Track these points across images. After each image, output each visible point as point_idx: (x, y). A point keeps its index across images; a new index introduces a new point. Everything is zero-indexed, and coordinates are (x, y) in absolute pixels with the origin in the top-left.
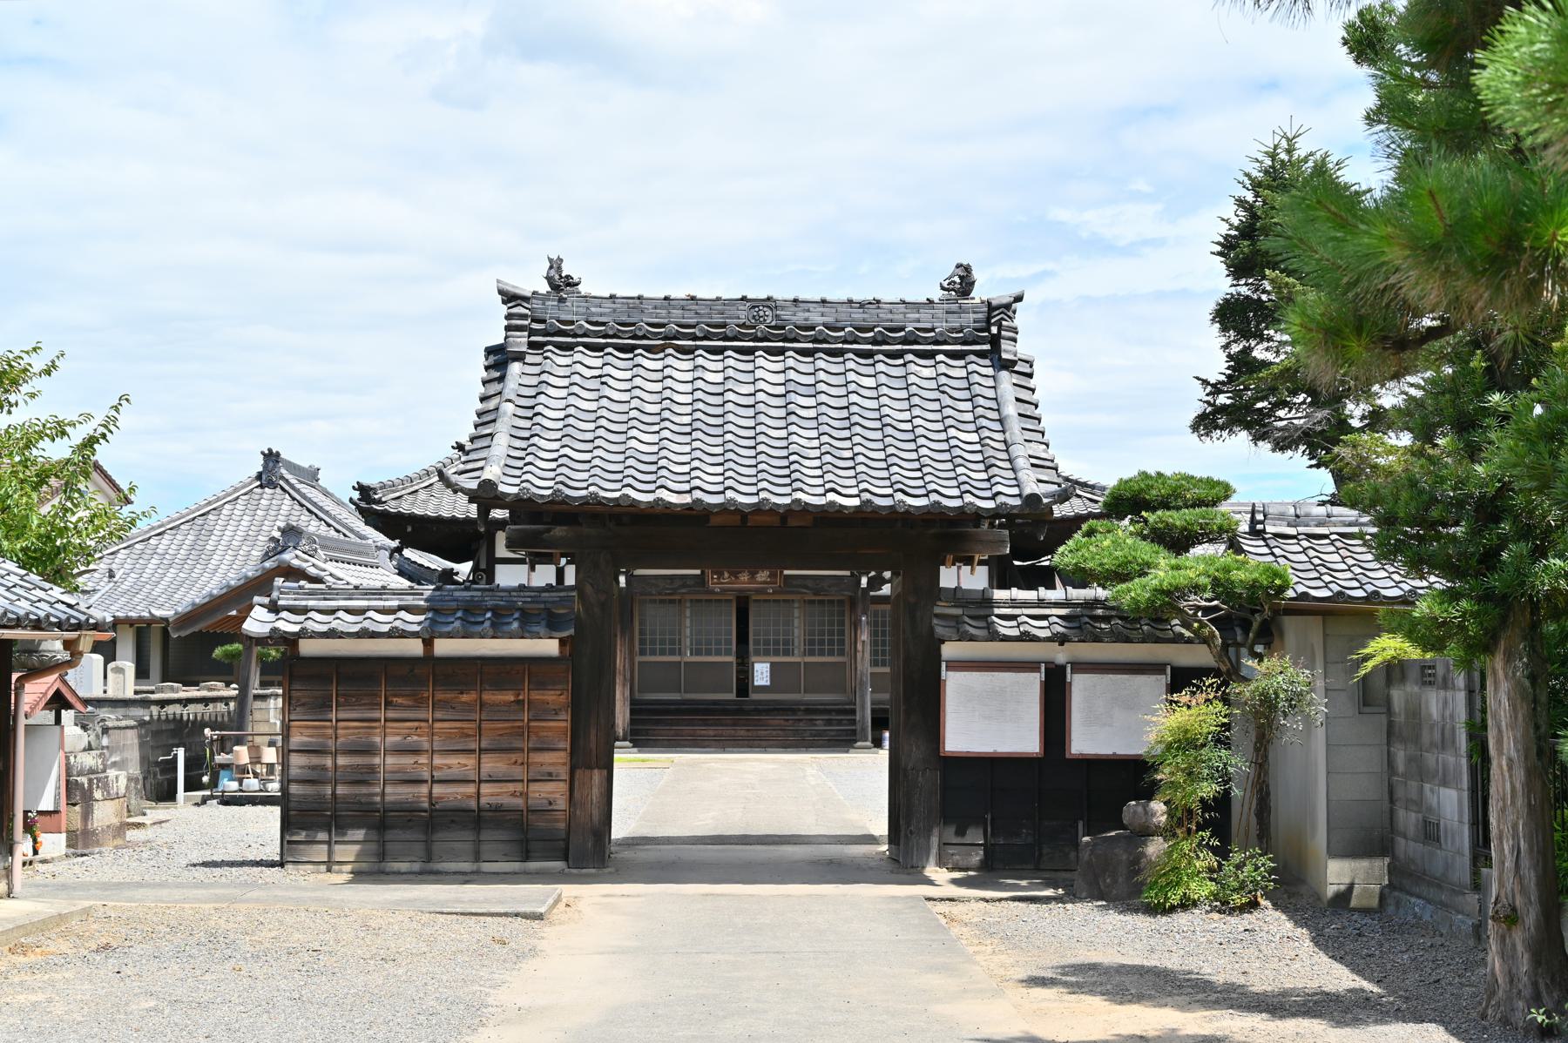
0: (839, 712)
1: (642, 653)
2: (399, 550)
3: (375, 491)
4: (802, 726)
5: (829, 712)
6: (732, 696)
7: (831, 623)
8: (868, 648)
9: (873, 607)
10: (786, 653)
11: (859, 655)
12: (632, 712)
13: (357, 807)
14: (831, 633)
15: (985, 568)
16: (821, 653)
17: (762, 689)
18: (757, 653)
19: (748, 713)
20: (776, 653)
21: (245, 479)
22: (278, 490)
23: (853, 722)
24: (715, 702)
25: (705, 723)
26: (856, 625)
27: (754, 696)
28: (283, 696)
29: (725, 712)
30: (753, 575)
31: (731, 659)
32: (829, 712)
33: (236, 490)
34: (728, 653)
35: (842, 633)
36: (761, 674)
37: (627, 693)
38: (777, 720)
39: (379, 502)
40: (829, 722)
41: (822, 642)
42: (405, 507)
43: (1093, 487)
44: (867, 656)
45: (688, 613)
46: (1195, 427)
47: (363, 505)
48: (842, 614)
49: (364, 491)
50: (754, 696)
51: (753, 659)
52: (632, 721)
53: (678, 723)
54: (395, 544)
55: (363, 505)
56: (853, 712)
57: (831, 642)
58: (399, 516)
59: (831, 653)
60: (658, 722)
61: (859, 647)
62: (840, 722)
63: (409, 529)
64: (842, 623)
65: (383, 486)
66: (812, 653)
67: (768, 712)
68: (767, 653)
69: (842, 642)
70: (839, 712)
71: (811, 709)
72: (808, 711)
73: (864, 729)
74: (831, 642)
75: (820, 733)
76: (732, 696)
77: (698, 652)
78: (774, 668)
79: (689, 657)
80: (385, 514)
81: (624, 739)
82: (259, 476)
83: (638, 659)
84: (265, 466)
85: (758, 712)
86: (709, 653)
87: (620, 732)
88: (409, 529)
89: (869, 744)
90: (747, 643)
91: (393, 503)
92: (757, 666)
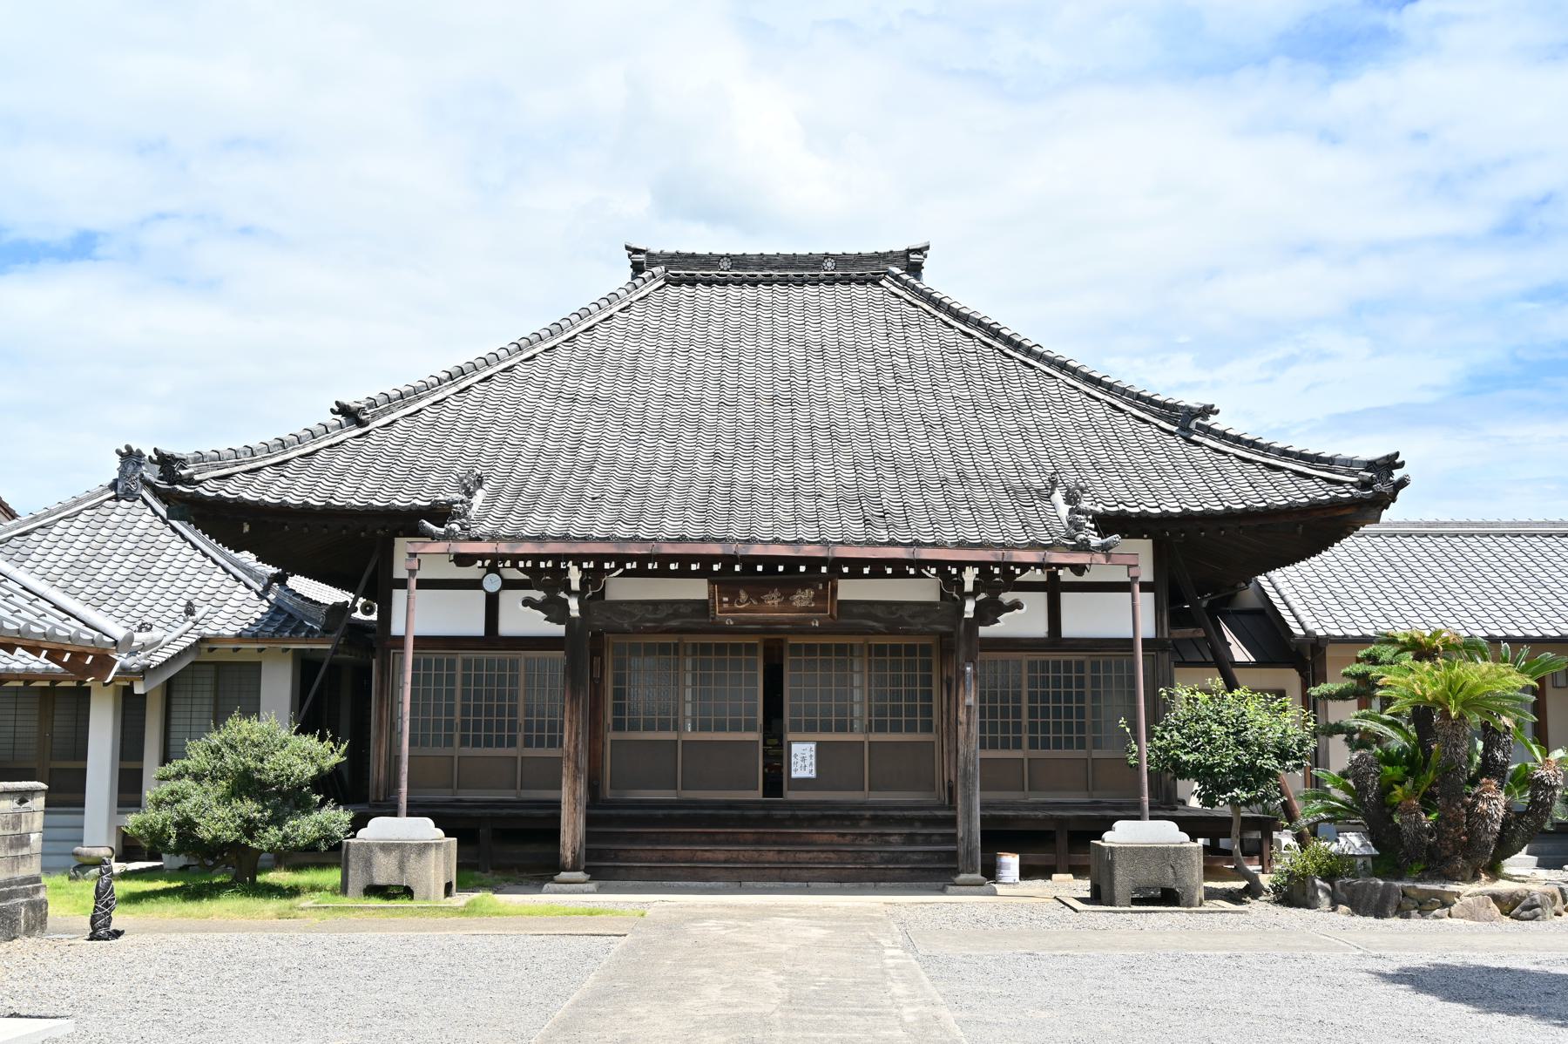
0: (926, 822)
1: (618, 726)
2: (281, 579)
3: (183, 463)
4: (867, 845)
5: (909, 821)
6: (758, 795)
7: (911, 680)
8: (976, 718)
9: (981, 656)
10: (842, 727)
11: (962, 730)
12: (590, 820)
13: (712, 873)
14: (911, 696)
15: (1150, 596)
16: (896, 728)
17: (803, 783)
18: (796, 727)
19: (780, 822)
20: (826, 728)
21: (94, 487)
22: (139, 503)
23: (953, 838)
24: (730, 805)
25: (712, 840)
26: (952, 685)
27: (790, 795)
28: (47, 793)
29: (744, 821)
30: (787, 597)
31: (756, 736)
32: (909, 821)
33: (78, 502)
34: (750, 727)
35: (928, 696)
36: (803, 759)
37: (582, 789)
38: (826, 835)
39: (189, 481)
40: (910, 839)
41: (896, 711)
42: (230, 490)
43: (1331, 461)
44: (975, 730)
45: (689, 663)
46: (1391, 462)
47: (163, 485)
48: (927, 666)
49: (166, 462)
50: (790, 795)
51: (789, 736)
52: (590, 836)
53: (668, 839)
54: (272, 570)
55: (163, 485)
56: (952, 822)
57: (911, 711)
58: (219, 502)
59: (911, 728)
60: (633, 839)
61: (962, 716)
62: (928, 839)
63: (246, 529)
64: (927, 681)
65: (200, 458)
66: (881, 727)
67: (811, 821)
68: (811, 727)
69: (928, 711)
70: (926, 822)
71: (882, 818)
72: (876, 820)
73: (969, 853)
74: (911, 711)
75: (896, 858)
76: (758, 795)
77: (705, 727)
78: (821, 748)
79: (689, 734)
80: (197, 500)
81: (575, 869)
82: (113, 486)
83: (611, 736)
84: (122, 471)
85: (797, 821)
86: (720, 727)
87: (567, 854)
88: (246, 529)
89: (978, 876)
90: (780, 715)
91: (213, 484)
92: (795, 748)
